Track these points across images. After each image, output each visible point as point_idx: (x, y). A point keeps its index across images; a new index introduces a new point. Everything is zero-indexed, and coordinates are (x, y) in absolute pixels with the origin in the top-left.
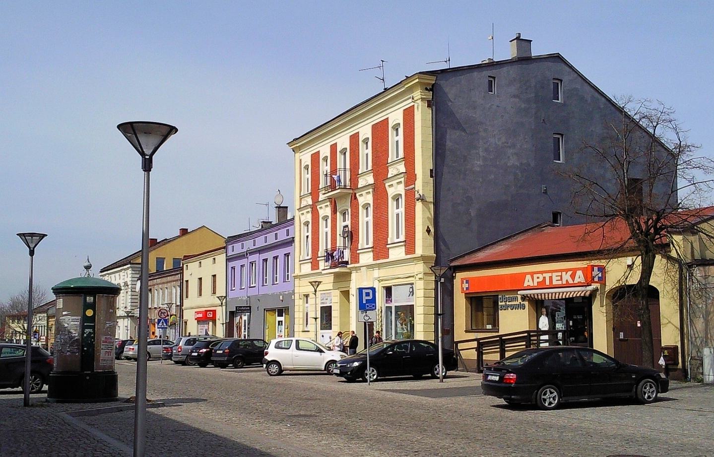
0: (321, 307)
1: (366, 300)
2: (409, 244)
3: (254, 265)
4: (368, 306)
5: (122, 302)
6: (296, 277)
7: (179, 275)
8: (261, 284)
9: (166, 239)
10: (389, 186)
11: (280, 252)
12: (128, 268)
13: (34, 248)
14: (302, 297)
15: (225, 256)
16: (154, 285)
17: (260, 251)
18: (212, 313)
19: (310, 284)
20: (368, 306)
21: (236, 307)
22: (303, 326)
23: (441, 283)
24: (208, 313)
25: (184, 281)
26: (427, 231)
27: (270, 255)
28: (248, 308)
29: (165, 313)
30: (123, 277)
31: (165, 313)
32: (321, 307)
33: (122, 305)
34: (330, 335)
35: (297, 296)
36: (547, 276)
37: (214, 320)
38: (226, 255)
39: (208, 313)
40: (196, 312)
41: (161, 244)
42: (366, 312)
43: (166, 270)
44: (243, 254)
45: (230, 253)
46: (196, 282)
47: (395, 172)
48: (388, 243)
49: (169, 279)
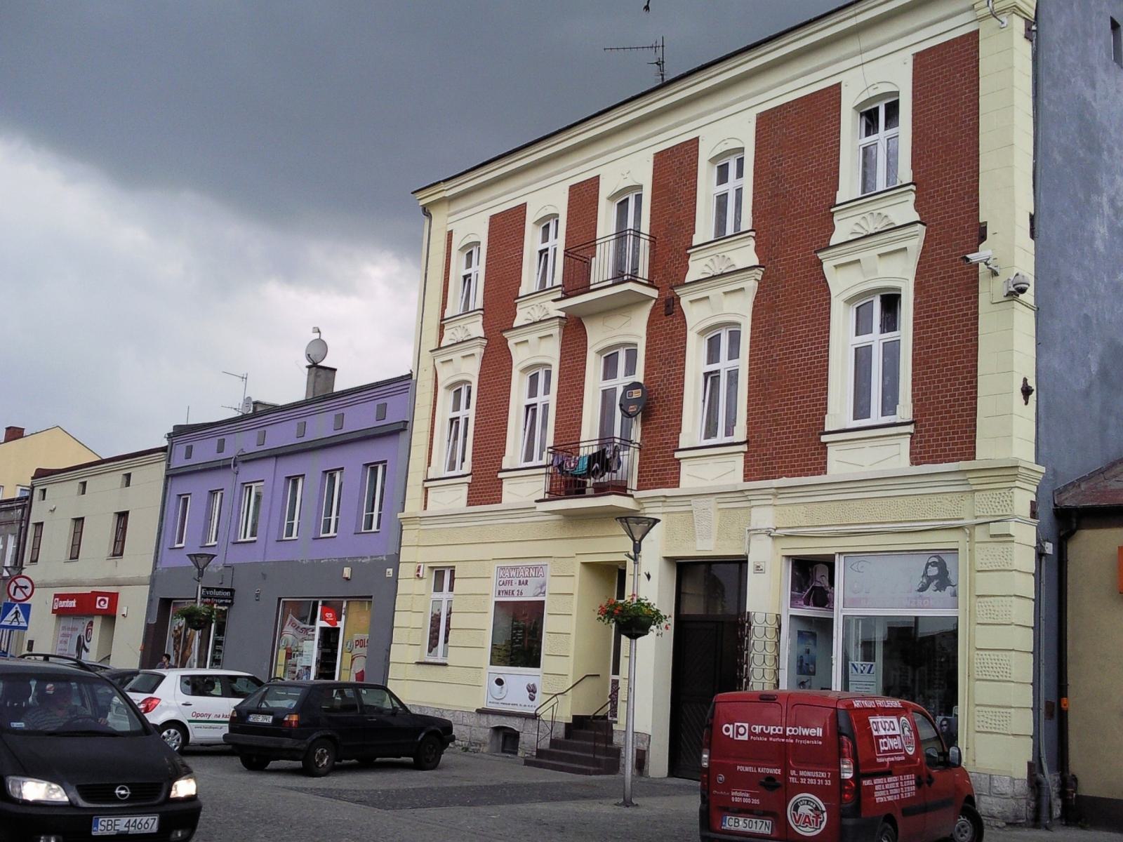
0: (496, 602)
2: (889, 404)
7: (20, 510)
10: (516, 344)
11: (352, 460)
14: (425, 571)
15: (164, 468)
17: (279, 454)
18: (107, 599)
19: (188, 558)
24: (99, 598)
25: (31, 526)
26: (1023, 391)
27: (313, 466)
28: (228, 594)
29: (26, 587)
31: (26, 587)
32: (496, 602)
35: (405, 571)
37: (110, 616)
38: (169, 465)
39: (99, 598)
40: (56, 596)
45: (179, 461)
46: (67, 528)
47: (460, 336)
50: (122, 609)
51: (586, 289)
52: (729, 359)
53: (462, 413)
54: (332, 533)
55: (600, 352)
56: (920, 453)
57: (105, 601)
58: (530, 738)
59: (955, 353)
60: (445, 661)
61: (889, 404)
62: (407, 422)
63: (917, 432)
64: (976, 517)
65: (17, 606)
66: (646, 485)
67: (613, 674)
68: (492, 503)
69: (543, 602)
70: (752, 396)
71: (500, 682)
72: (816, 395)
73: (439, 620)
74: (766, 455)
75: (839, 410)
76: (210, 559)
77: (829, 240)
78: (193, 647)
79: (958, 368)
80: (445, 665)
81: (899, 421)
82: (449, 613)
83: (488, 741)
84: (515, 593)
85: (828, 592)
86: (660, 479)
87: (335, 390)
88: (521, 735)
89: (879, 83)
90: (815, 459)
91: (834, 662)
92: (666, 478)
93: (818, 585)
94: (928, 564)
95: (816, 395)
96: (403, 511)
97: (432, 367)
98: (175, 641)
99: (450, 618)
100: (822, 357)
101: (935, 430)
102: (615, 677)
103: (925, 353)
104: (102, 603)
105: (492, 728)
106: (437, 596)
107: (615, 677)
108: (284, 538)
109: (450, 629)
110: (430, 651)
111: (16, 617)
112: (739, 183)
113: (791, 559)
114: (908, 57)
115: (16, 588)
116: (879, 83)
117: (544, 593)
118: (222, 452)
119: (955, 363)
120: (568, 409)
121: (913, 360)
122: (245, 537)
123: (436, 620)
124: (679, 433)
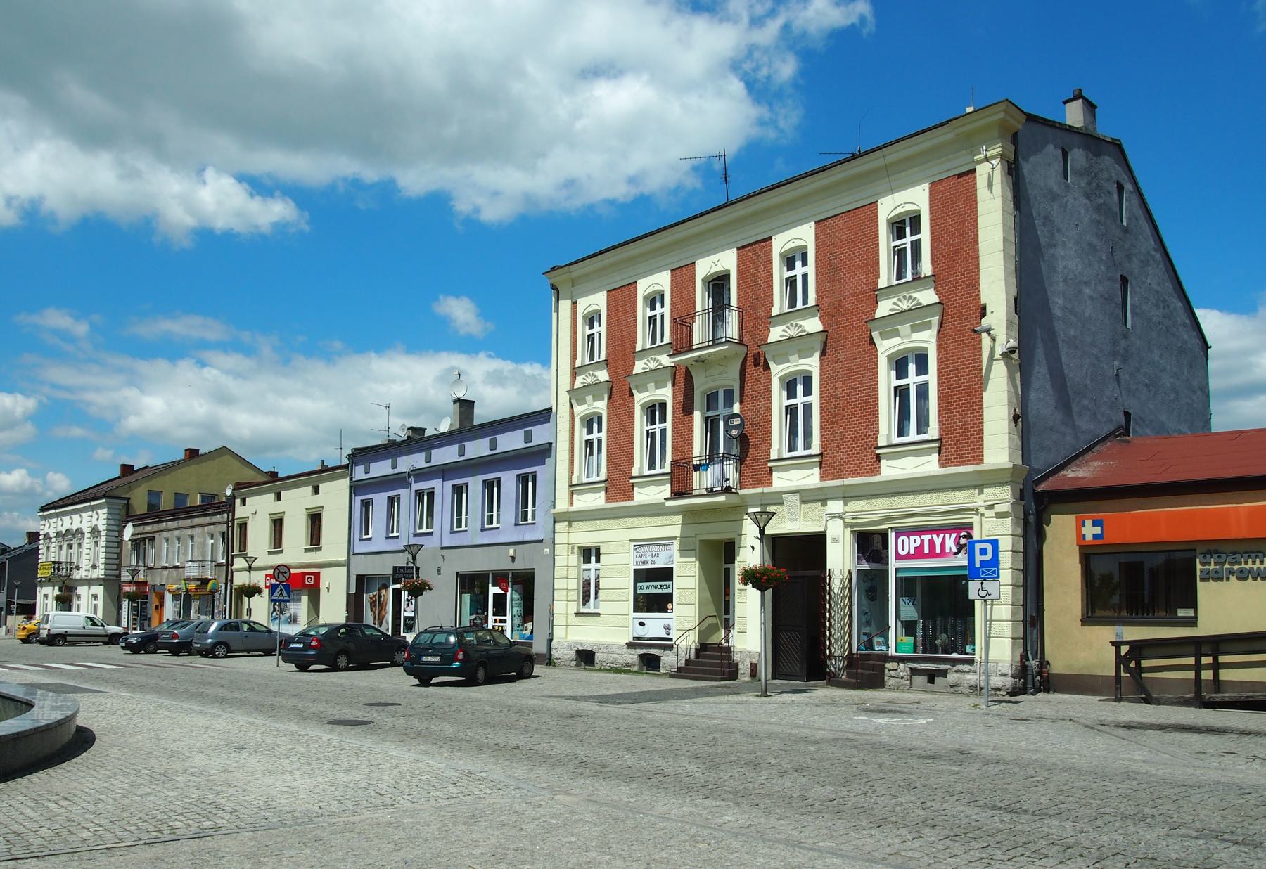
0: (634, 570)
1: (981, 561)
2: (923, 426)
4: (983, 573)
5: (88, 557)
6: (557, 519)
8: (447, 527)
12: (99, 507)
13: (764, 527)
16: (162, 531)
18: (312, 577)
20: (983, 573)
22: (578, 605)
23: (742, 483)
24: (307, 577)
29: (285, 573)
30: (89, 519)
31: (285, 573)
32: (634, 570)
33: (87, 562)
34: (667, 622)
36: (926, 538)
38: (351, 479)
39: (307, 577)
42: (982, 583)
43: (190, 507)
44: (403, 475)
48: (879, 445)
49: (197, 521)
50: (324, 584)
51: (689, 349)
52: (788, 399)
53: (595, 436)
54: (495, 525)
55: (781, 379)
56: (946, 460)
57: (308, 578)
58: (669, 660)
59: (967, 393)
60: (597, 612)
62: (551, 443)
64: (985, 501)
65: (281, 585)
66: (747, 485)
67: (725, 614)
68: (626, 500)
69: (672, 568)
70: (823, 422)
71: (642, 624)
72: (870, 422)
73: (589, 584)
74: (836, 462)
75: (886, 429)
76: (770, 516)
77: (874, 313)
78: (387, 608)
79: (969, 403)
80: (598, 615)
81: (930, 439)
82: (598, 578)
83: (637, 664)
84: (650, 563)
85: (881, 553)
86: (757, 481)
87: (475, 424)
88: (662, 658)
89: (905, 203)
90: (872, 465)
91: (890, 599)
92: (761, 480)
93: (875, 548)
95: (870, 422)
96: (554, 508)
97: (568, 403)
98: (371, 605)
99: (599, 582)
100: (873, 395)
101: (955, 444)
102: (727, 617)
103: (946, 393)
104: (309, 579)
105: (639, 655)
106: (586, 566)
107: (727, 617)
108: (521, 523)
109: (599, 589)
110: (584, 605)
111: (281, 593)
112: (805, 270)
113: (893, 530)
115: (278, 573)
116: (905, 203)
117: (672, 561)
118: (369, 473)
119: (967, 400)
120: (682, 433)
122: (393, 532)
123: (587, 584)
124: (769, 449)
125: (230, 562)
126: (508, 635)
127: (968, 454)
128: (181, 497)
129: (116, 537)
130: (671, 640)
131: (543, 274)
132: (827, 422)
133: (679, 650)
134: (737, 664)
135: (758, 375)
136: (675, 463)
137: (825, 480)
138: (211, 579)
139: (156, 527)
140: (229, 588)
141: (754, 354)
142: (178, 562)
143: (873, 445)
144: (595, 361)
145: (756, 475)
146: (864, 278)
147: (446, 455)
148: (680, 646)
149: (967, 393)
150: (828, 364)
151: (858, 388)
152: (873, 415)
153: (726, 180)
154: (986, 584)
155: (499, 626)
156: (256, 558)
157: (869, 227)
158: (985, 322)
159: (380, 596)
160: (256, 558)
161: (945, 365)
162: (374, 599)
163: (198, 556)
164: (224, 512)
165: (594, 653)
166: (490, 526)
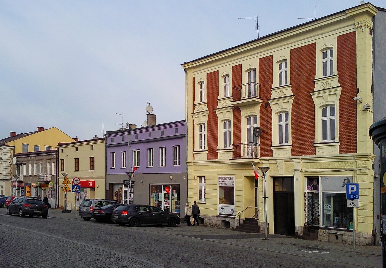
2: (333, 137)
3: (124, 153)
4: (353, 196)
9: (22, 134)
11: (169, 145)
13: (265, 173)
18: (91, 183)
20: (353, 196)
21: (124, 181)
24: (89, 183)
29: (78, 181)
31: (78, 181)
39: (89, 183)
41: (19, 136)
42: (352, 201)
46: (74, 162)
50: (96, 186)
54: (164, 166)
57: (90, 183)
58: (233, 224)
59: (351, 124)
61: (333, 137)
63: (341, 145)
71: (222, 208)
84: (225, 184)
85: (317, 186)
94: (345, 180)
96: (187, 160)
107: (257, 208)
108: (148, 167)
110: (200, 200)
111: (77, 189)
114: (335, 37)
115: (75, 181)
121: (339, 125)
122: (123, 166)
123: (201, 191)
125: (57, 175)
126: (170, 211)
127: (351, 148)
128: (37, 147)
129: (9, 162)
130: (234, 215)
131: (181, 65)
132: (294, 132)
133: (237, 220)
134: (260, 227)
135: (267, 112)
136: (234, 145)
137: (293, 156)
138: (50, 182)
139: (26, 159)
140: (57, 186)
141: (265, 103)
142: (36, 174)
143: (313, 143)
144: (202, 102)
145: (266, 152)
146: (310, 74)
147: (144, 136)
148: (237, 218)
149: (351, 124)
150: (295, 109)
151: (307, 119)
152: (313, 130)
153: (258, 28)
154: (354, 201)
155: (166, 206)
156: (67, 174)
157: (312, 53)
158: (359, 96)
159: (119, 192)
160: (67, 174)
161: (342, 112)
162: (117, 193)
163: (44, 172)
164: (54, 154)
165: (204, 219)
166: (162, 166)
